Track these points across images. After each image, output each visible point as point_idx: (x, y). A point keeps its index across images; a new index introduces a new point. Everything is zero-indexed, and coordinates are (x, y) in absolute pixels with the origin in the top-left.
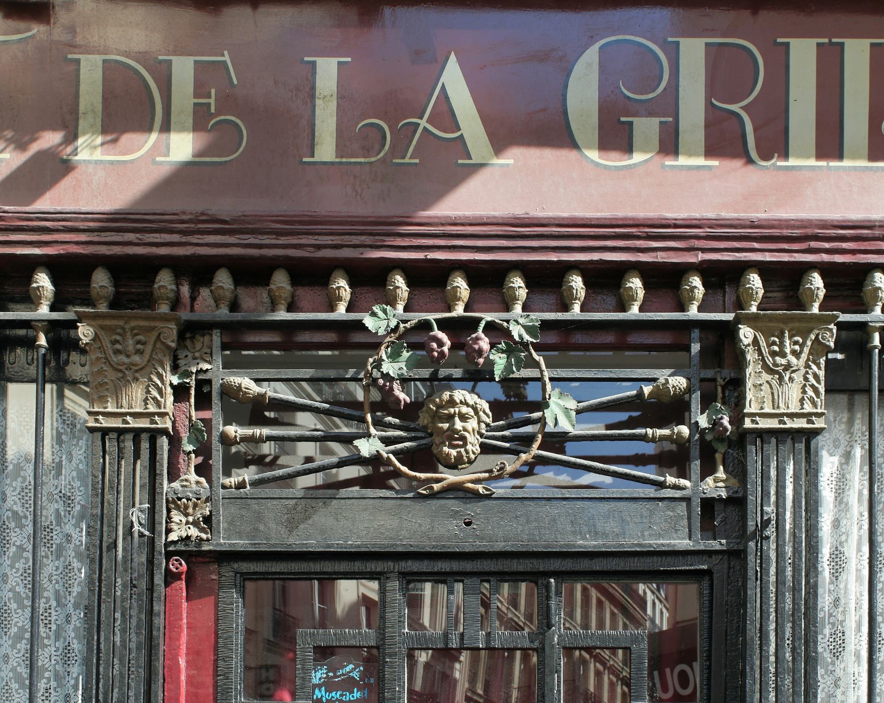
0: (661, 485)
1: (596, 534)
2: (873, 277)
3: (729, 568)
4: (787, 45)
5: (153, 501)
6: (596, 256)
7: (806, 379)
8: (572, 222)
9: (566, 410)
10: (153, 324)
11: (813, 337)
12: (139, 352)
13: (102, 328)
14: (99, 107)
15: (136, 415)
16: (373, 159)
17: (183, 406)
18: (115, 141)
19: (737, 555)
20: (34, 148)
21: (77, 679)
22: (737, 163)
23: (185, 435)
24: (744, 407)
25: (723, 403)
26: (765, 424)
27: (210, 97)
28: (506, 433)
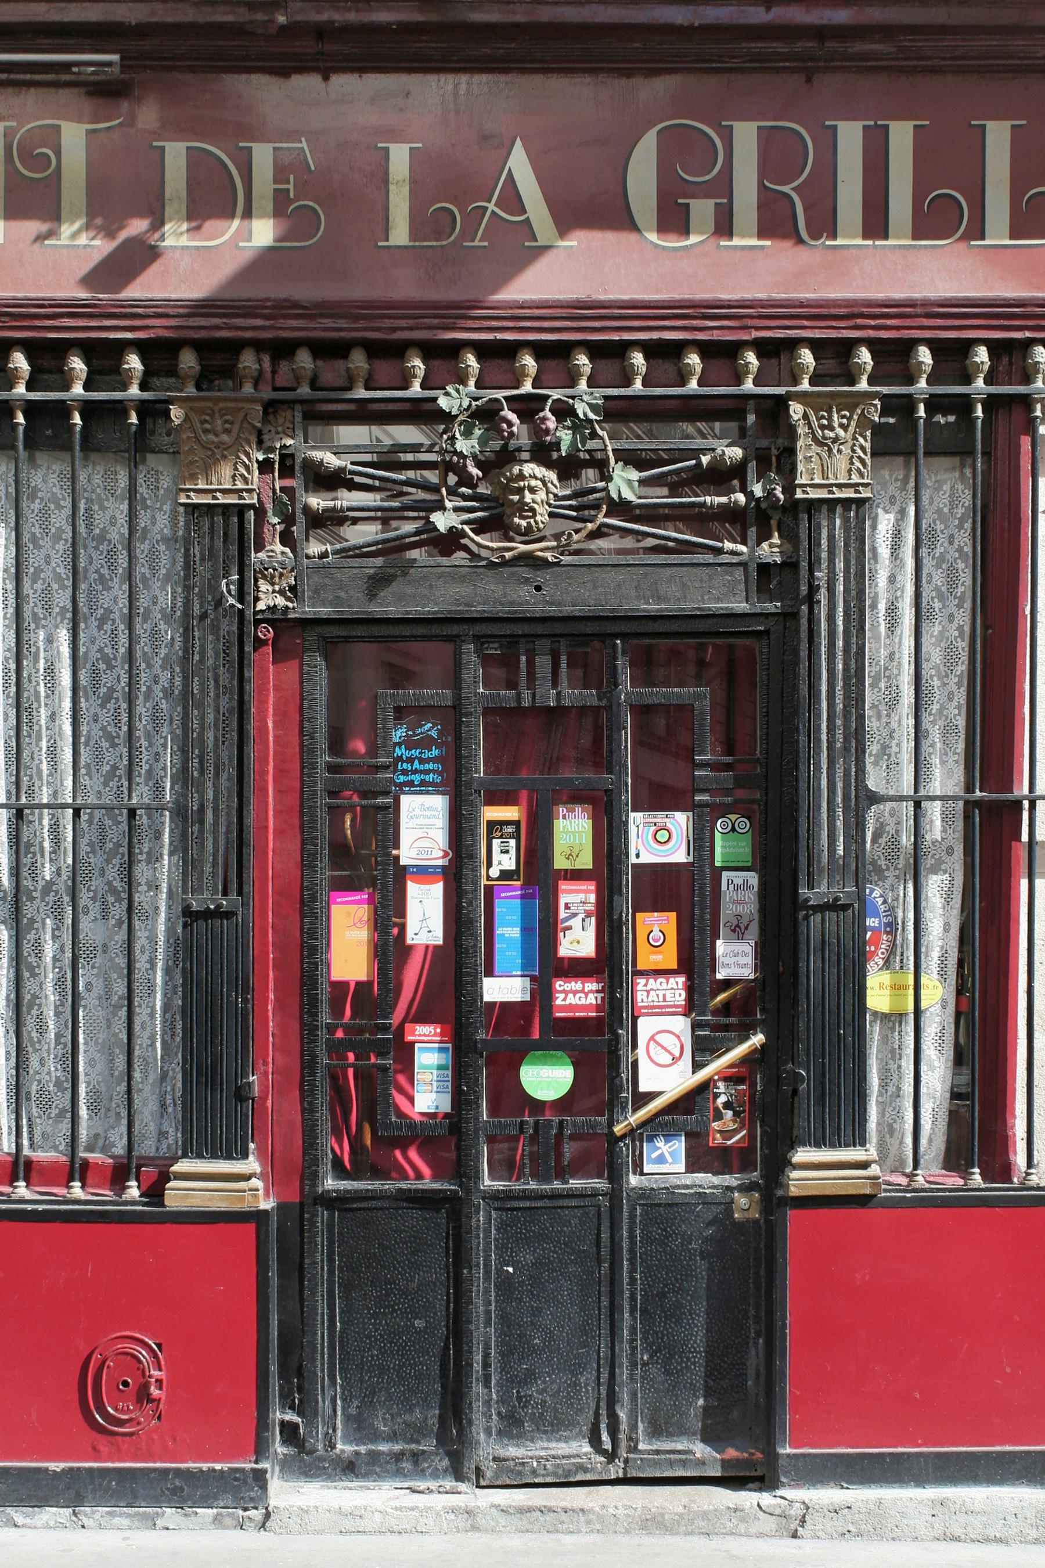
0: (719, 551)
1: (659, 599)
2: (918, 351)
3: (785, 628)
4: (835, 127)
5: (241, 573)
6: (655, 335)
7: (853, 451)
8: (631, 304)
9: (629, 482)
10: (240, 405)
11: (859, 411)
12: (227, 431)
13: (191, 409)
14: (184, 194)
15: (225, 492)
16: (444, 243)
17: (268, 478)
18: (198, 228)
19: (789, 616)
20: (123, 235)
21: (166, 738)
22: (787, 244)
23: (269, 506)
24: (795, 478)
25: (777, 474)
26: (814, 494)
27: (288, 183)
28: (573, 503)
